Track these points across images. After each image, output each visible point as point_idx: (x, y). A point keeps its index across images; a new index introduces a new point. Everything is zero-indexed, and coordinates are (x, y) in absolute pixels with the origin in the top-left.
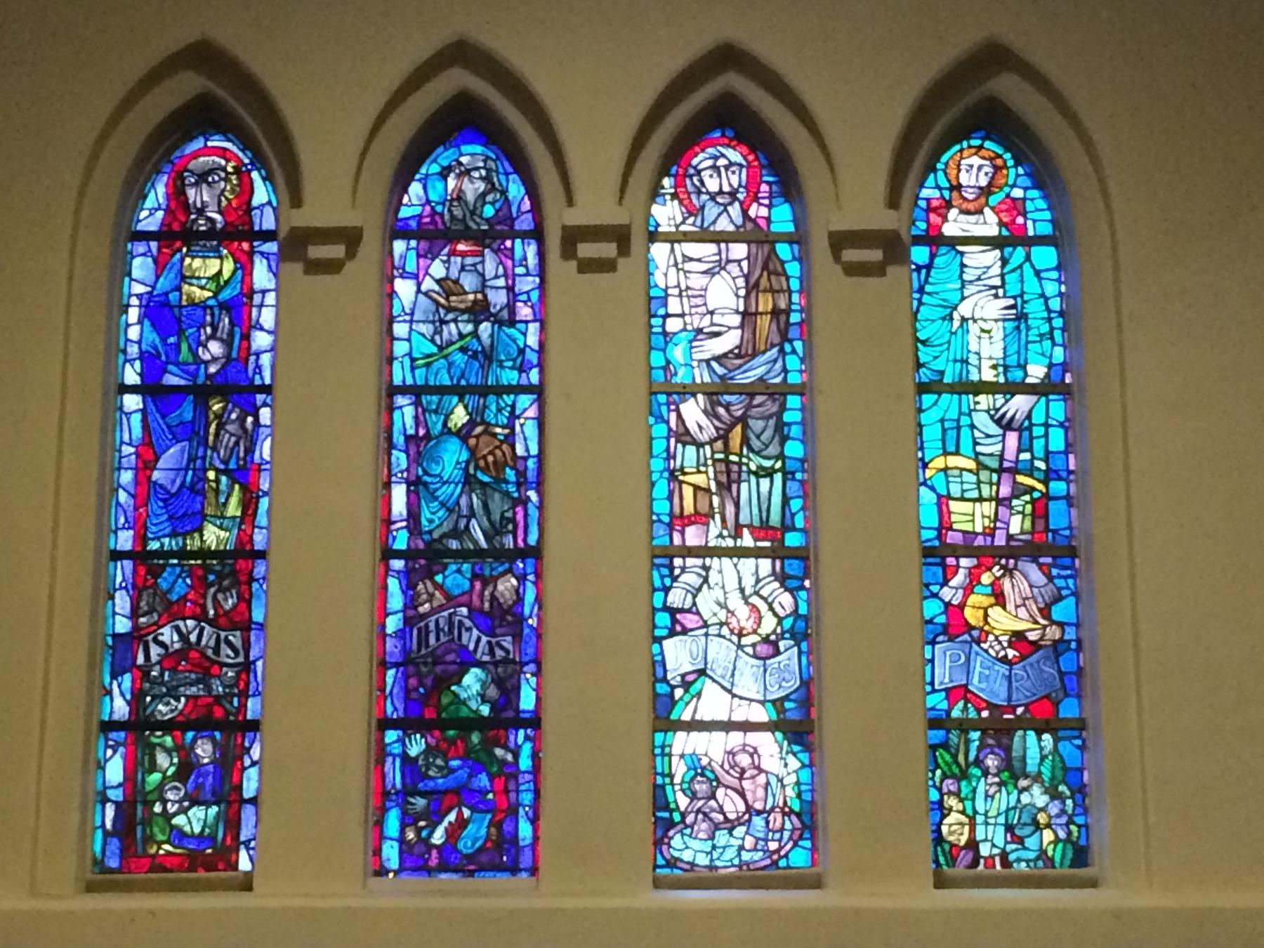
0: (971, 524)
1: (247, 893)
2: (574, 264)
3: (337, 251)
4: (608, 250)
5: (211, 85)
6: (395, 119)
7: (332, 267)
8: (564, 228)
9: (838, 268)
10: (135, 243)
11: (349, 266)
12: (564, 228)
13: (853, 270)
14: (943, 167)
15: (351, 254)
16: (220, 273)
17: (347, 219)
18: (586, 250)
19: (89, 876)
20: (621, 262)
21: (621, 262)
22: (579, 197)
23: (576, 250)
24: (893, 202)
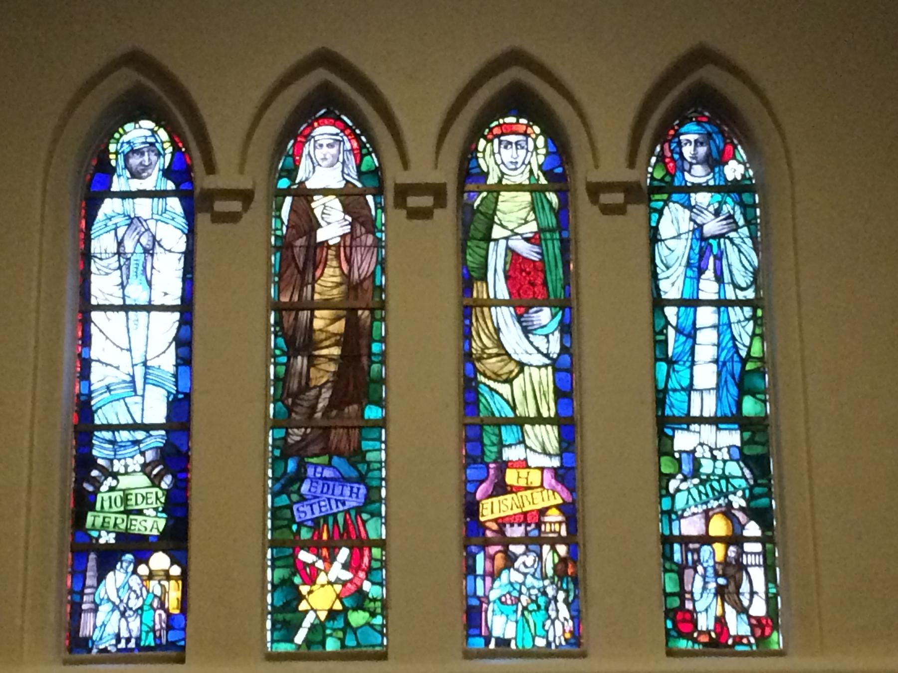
0: (705, 394)
1: (179, 666)
2: (404, 212)
3: (427, 201)
4: (235, 206)
5: (143, 79)
6: (269, 114)
7: (233, 218)
8: (396, 185)
9: (596, 209)
10: (763, 415)
11: (246, 217)
12: (396, 185)
13: (607, 210)
14: (539, 151)
15: (246, 208)
16: (488, 348)
17: (244, 183)
18: (413, 201)
19: (63, 655)
20: (437, 212)
21: (437, 212)
22: (413, 165)
23: (598, 198)
24: (632, 164)
